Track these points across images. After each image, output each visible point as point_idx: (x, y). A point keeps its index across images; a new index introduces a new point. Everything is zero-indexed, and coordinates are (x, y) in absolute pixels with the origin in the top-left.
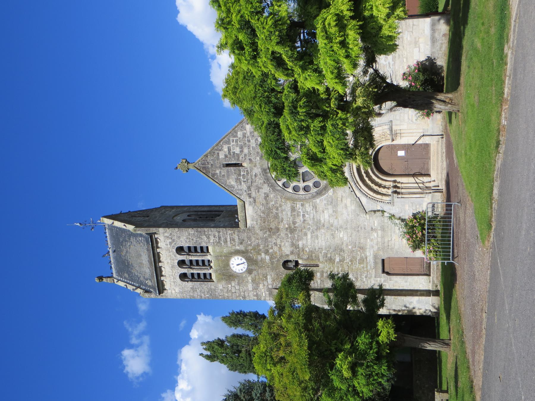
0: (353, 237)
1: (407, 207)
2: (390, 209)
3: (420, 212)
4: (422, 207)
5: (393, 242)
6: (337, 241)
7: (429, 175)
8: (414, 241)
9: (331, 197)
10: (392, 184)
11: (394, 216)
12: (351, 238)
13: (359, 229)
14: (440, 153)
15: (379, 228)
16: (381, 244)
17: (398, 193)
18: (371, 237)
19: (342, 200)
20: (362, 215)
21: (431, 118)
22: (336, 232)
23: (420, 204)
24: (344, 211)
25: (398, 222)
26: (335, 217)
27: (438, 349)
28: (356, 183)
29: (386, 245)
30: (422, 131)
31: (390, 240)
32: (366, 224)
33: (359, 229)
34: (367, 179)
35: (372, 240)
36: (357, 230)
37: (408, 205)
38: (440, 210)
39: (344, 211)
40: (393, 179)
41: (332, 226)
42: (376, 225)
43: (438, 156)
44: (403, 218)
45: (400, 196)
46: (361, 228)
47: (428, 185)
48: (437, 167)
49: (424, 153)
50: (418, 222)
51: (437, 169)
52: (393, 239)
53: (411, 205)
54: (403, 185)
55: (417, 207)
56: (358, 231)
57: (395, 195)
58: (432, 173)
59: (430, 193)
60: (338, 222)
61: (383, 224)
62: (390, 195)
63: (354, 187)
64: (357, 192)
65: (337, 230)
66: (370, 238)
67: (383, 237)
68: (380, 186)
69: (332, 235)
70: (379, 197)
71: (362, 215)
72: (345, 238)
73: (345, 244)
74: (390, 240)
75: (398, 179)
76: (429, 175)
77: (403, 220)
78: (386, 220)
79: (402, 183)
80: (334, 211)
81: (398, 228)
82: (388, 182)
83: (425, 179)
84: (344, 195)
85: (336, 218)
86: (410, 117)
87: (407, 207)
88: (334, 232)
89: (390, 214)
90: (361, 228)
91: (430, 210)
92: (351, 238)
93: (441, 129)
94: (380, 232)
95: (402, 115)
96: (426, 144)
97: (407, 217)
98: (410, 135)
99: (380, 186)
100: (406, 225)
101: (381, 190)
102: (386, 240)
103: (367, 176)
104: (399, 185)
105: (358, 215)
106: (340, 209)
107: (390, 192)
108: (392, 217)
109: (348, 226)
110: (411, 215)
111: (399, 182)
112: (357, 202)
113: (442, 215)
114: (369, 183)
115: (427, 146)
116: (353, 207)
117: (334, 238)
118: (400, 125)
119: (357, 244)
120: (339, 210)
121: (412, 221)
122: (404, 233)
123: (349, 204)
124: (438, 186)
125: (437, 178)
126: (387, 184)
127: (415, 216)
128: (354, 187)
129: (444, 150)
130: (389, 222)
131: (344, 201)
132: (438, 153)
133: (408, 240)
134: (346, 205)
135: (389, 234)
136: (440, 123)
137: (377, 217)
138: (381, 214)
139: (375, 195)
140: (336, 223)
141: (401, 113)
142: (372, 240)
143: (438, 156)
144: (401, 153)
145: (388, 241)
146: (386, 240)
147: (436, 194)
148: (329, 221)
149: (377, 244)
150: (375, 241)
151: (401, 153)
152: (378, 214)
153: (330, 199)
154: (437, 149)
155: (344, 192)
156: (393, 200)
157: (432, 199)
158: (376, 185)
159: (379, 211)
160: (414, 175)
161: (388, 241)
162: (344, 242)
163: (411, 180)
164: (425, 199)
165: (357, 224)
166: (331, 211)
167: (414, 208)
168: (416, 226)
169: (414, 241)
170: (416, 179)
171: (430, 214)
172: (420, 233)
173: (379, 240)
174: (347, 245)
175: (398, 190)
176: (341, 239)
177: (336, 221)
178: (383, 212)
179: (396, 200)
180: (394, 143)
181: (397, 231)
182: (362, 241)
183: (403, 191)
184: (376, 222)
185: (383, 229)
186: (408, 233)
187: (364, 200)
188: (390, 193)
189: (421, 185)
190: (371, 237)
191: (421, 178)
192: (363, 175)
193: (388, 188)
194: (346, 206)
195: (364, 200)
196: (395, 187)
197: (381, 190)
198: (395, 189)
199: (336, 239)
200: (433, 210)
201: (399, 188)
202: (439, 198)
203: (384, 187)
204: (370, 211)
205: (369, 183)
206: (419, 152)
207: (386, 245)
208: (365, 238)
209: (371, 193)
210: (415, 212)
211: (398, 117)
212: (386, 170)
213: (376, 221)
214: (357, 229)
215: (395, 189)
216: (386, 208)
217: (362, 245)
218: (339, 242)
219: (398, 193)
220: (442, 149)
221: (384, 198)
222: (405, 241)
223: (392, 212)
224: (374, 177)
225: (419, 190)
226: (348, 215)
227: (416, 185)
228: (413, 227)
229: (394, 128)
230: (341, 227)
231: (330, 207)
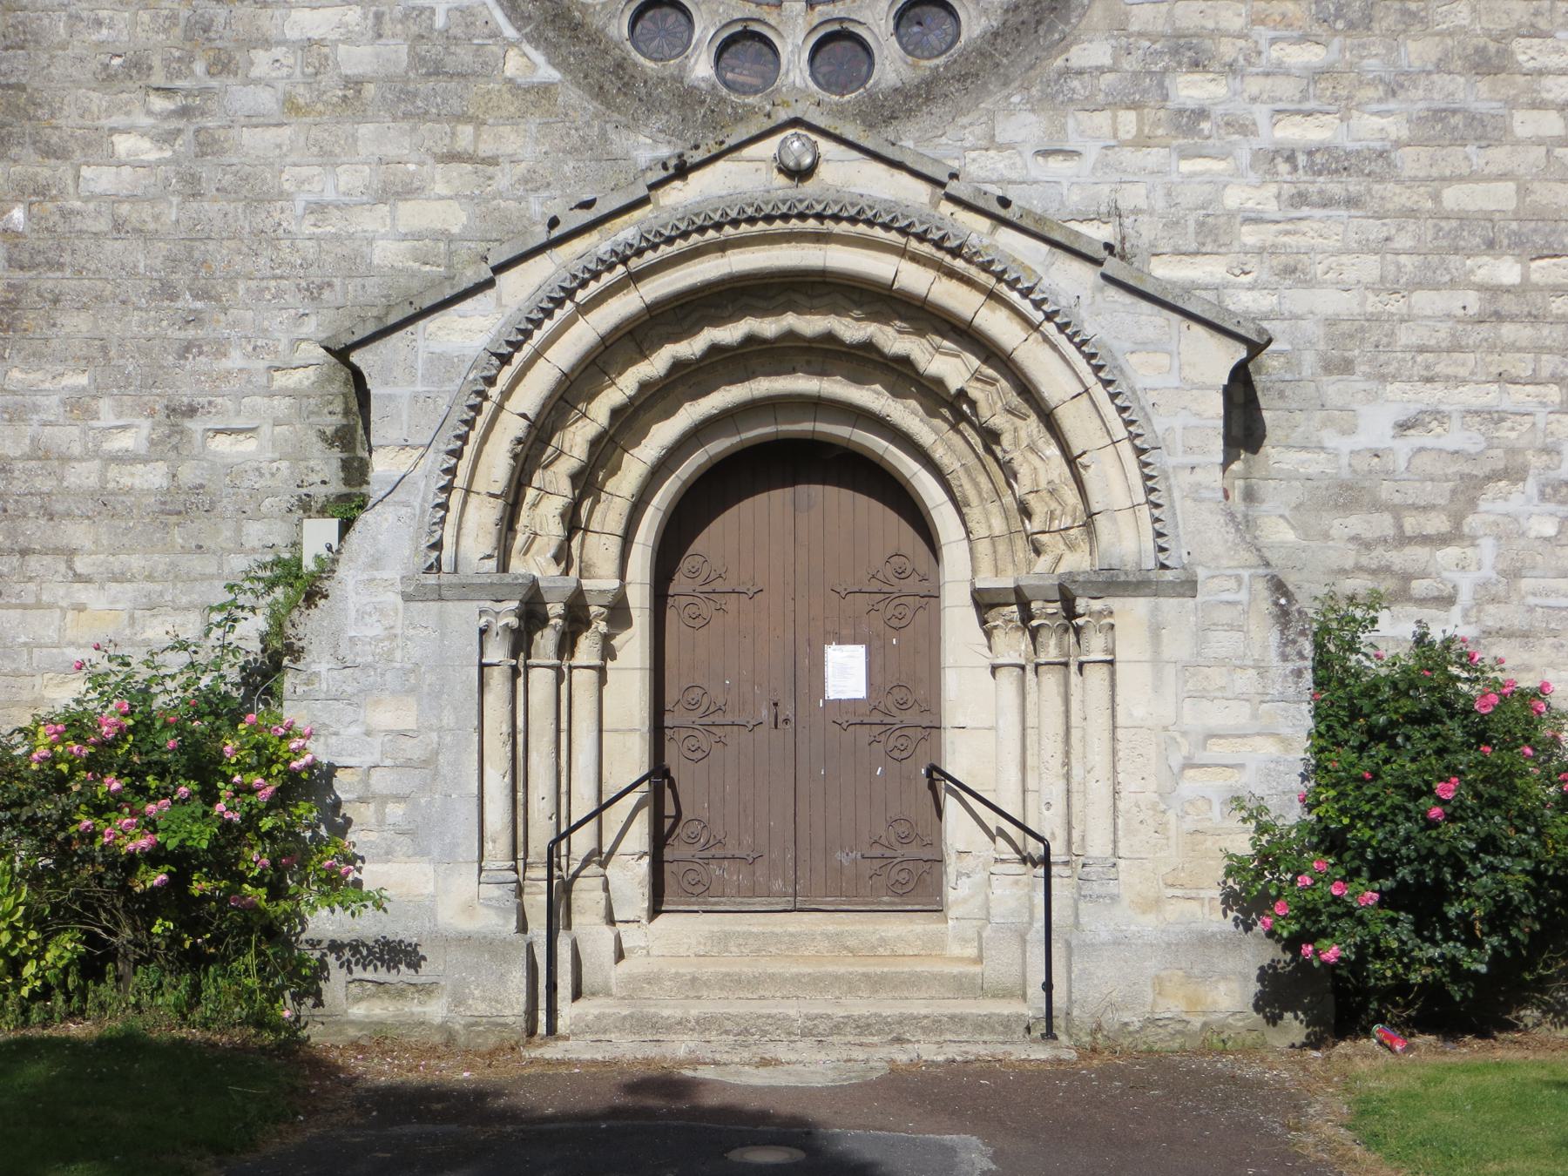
0: (112, 247)
1: (390, 715)
2: (376, 562)
3: (342, 829)
4: (387, 855)
5: (57, 591)
6: (78, 106)
7: (656, 910)
8: (60, 784)
9: (488, 69)
10: (602, 582)
11: (312, 596)
12: (103, 225)
13: (187, 302)
14: (889, 1007)
15: (189, 474)
16: (47, 485)
17: (521, 642)
18: (105, 406)
19: (452, 157)
20: (310, 327)
21: (1222, 923)
22: (159, 103)
23: (416, 837)
24: (350, 178)
25: (250, 631)
26: (303, 95)
27: (635, 613)
28: (629, 266)
29: (34, 530)
30: (1098, 846)
31: (81, 565)
32: (235, 360)
33: (187, 302)
34: (657, 364)
35: (79, 407)
36: (180, 279)
37: (409, 721)
38: (358, 1011)
39: (350, 178)
40: (639, 598)
41: (222, 65)
42: (222, 444)
43: (849, 984)
44: (289, 682)
45: (497, 652)
46: (194, 319)
47: (587, 894)
48: (753, 983)
49: (843, 858)
50: (251, 820)
51: (733, 983)
52: (83, 594)
53: (413, 750)
54: (583, 681)
55: (395, 811)
56: (168, 292)
57: (507, 614)
58: (682, 936)
59: (523, 927)
60: (255, 120)
61: (227, 505)
62: (504, 567)
63: (597, 244)
64: (522, 286)
65: (184, 112)
66: (99, 391)
67: (104, 503)
68: (587, 482)
69: (138, 65)
70: (497, 466)
71: (310, 327)
72: (99, 178)
73: (44, 171)
74: (81, 565)
75: (634, 645)
76: (656, 910)
77: (265, 676)
78: (264, 536)
79: (602, 671)
80: (355, 84)
81: (191, 632)
82: (616, 563)
83: (630, 874)
84: (504, 178)
85: (291, 106)
86: (1218, 751)
87: (390, 715)
88: (158, 79)
89: (327, 567)
90: (194, 319)
91: (366, 925)
92: (103, 225)
93: (1112, 1020)
94: (152, 477)
95: (1246, 681)
96: (939, 890)
97: (293, 712)
98: (520, 738)
99: (587, 482)
100: (220, 709)
101: (555, 481)
102: (77, 533)
103: (678, 365)
104: (587, 649)
105: (314, 293)
106: (378, 139)
107: (535, 564)
108: (304, 586)
109: (211, 208)
110: (319, 751)
111: (608, 652)
112: (433, 284)
113: (316, 1034)
114: (627, 384)
115: (914, 880)
116: (387, 253)
117: (107, 78)
118: (1157, 661)
119: (50, 281)
120: (365, 130)
121: (264, 758)
122: (146, 694)
123: (414, 215)
124: (577, 994)
125: (652, 979)
126: (600, 549)
127: (312, 784)
128: (597, 244)
129: (930, 1051)
130: (239, 563)
131: (443, 180)
132: (876, 983)
133: (75, 725)
134: (408, 191)
135: (136, 562)
136: (1171, 1006)
137: (296, 456)
138: (320, 493)
139: (511, 427)
140: (244, 98)
141: (1262, 671)
142: (79, 407)
143: (849, 984)
144: (846, 672)
145: (70, 553)
146: (77, 533)
147: (518, 977)
148: (267, 43)
149: (40, 454)
150: (68, 437)
151: (846, 672)
152: (325, 471)
153: (463, 56)
154: (913, 982)
155: (531, 182)
156: (467, 591)
157: (465, 941)
158: (595, 443)
159: (356, 471)
160: (659, 774)
161: (70, 553)
162: (64, 170)
163: (629, 759)
164: (465, 882)
165: (232, 280)
166: (357, 59)
167: (381, 782)
168: (210, 797)
169: (60, 784)
170: (632, 799)
171: (324, 922)
172: (143, 843)
173: (83, 475)
174: (42, 192)
175: (545, 641)
176: (96, 144)
177: (266, 100)
178: (348, 509)
179: (465, 616)
180: (958, 617)
181: (157, 631)
182: (76, 324)
183: (541, 682)
184: (248, 446)
185: (182, 506)
186: (144, 726)
187: (470, 330)
188: (517, 565)
189: (582, 842)
190: (105, 406)
191: (639, 836)
192: (690, 331)
193: (563, 555)
194: (394, 192)
195: (470, 330)
196: (577, 618)
197: (555, 481)
198: (555, 609)
199: (97, 100)
200: (357, 952)
201: (567, 645)
202: (482, 1008)
203: (572, 522)
204: (358, 378)
205: (627, 384)
206: (870, 817)
207: (34, 530)
208: (98, 353)
209: (531, 395)
210: (344, 786)
211: (1223, 643)
212: (699, 544)
213: (261, 439)
214: (190, 285)
215: (555, 609)
216: (388, 531)
217: (30, 319)
218: (69, 120)
219: (521, 642)
220: (933, 1026)
221: (482, 516)
222: (64, 694)
223: (348, 583)
224: (663, 434)
225: (541, 834)
226: (319, 209)
227: (583, 804)
228: (204, 769)
229: (1131, 612)
230: (206, 146)
231: (397, 52)
